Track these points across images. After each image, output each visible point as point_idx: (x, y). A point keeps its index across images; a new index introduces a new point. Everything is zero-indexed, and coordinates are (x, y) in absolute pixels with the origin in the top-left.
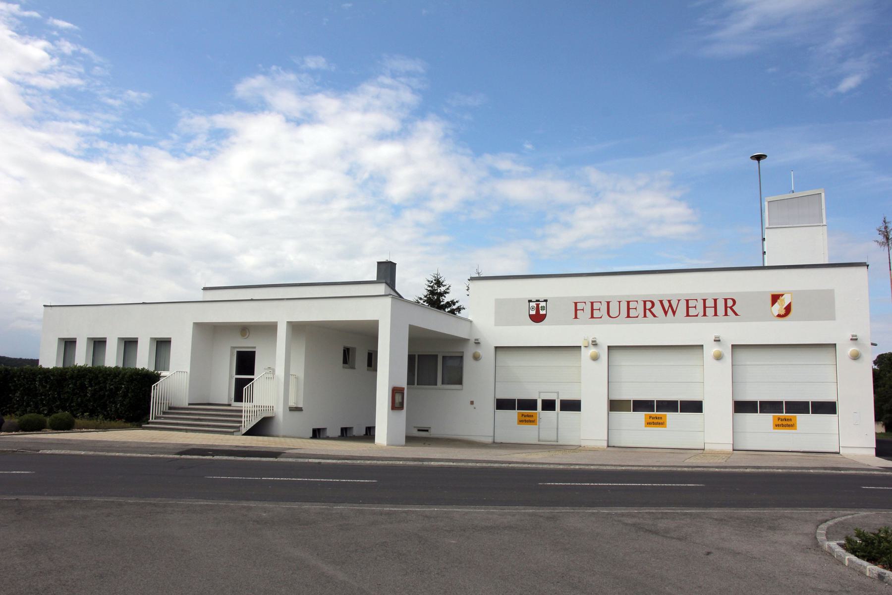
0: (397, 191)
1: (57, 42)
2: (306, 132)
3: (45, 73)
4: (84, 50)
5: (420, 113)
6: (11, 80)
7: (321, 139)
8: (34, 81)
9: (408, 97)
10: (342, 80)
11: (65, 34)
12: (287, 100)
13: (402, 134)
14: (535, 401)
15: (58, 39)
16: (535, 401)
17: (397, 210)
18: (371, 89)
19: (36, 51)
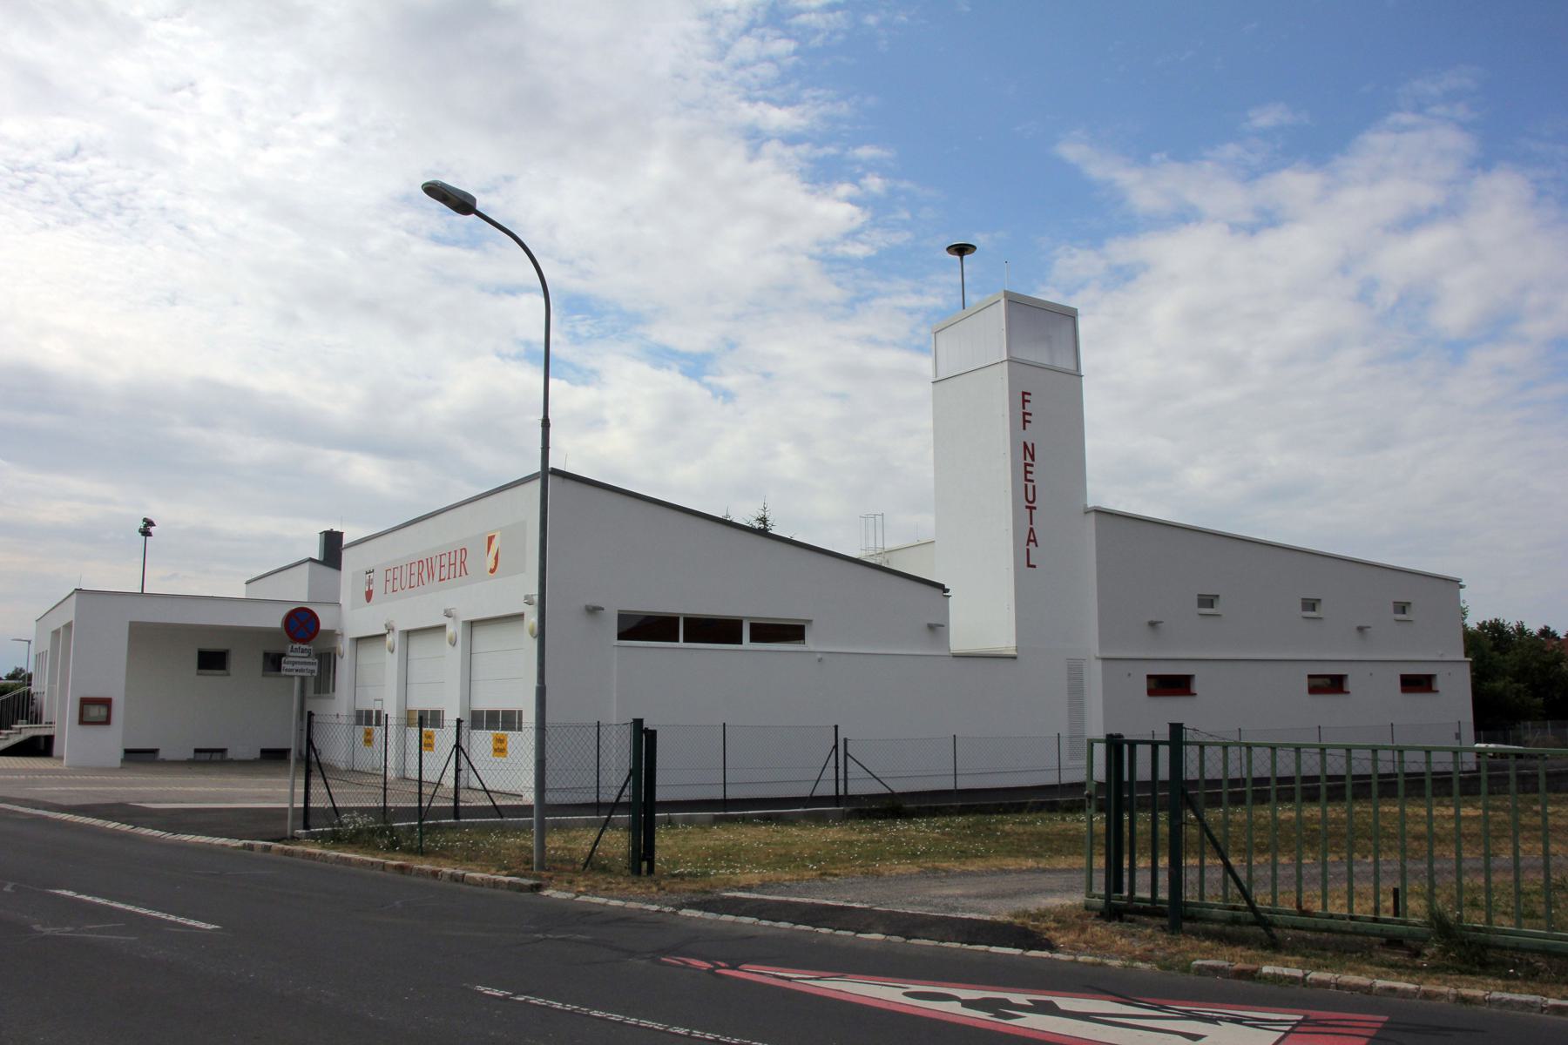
0: (1454, 316)
1: (863, 182)
2: (1269, 241)
3: (852, 236)
4: (904, 185)
5: (1484, 163)
6: (811, 257)
7: (1303, 245)
8: (839, 250)
9: (1451, 138)
10: (1320, 144)
11: (872, 167)
12: (1222, 195)
13: (1449, 210)
14: (753, 639)
15: (862, 176)
16: (753, 639)
17: (1456, 350)
18: (1377, 140)
19: (834, 211)
